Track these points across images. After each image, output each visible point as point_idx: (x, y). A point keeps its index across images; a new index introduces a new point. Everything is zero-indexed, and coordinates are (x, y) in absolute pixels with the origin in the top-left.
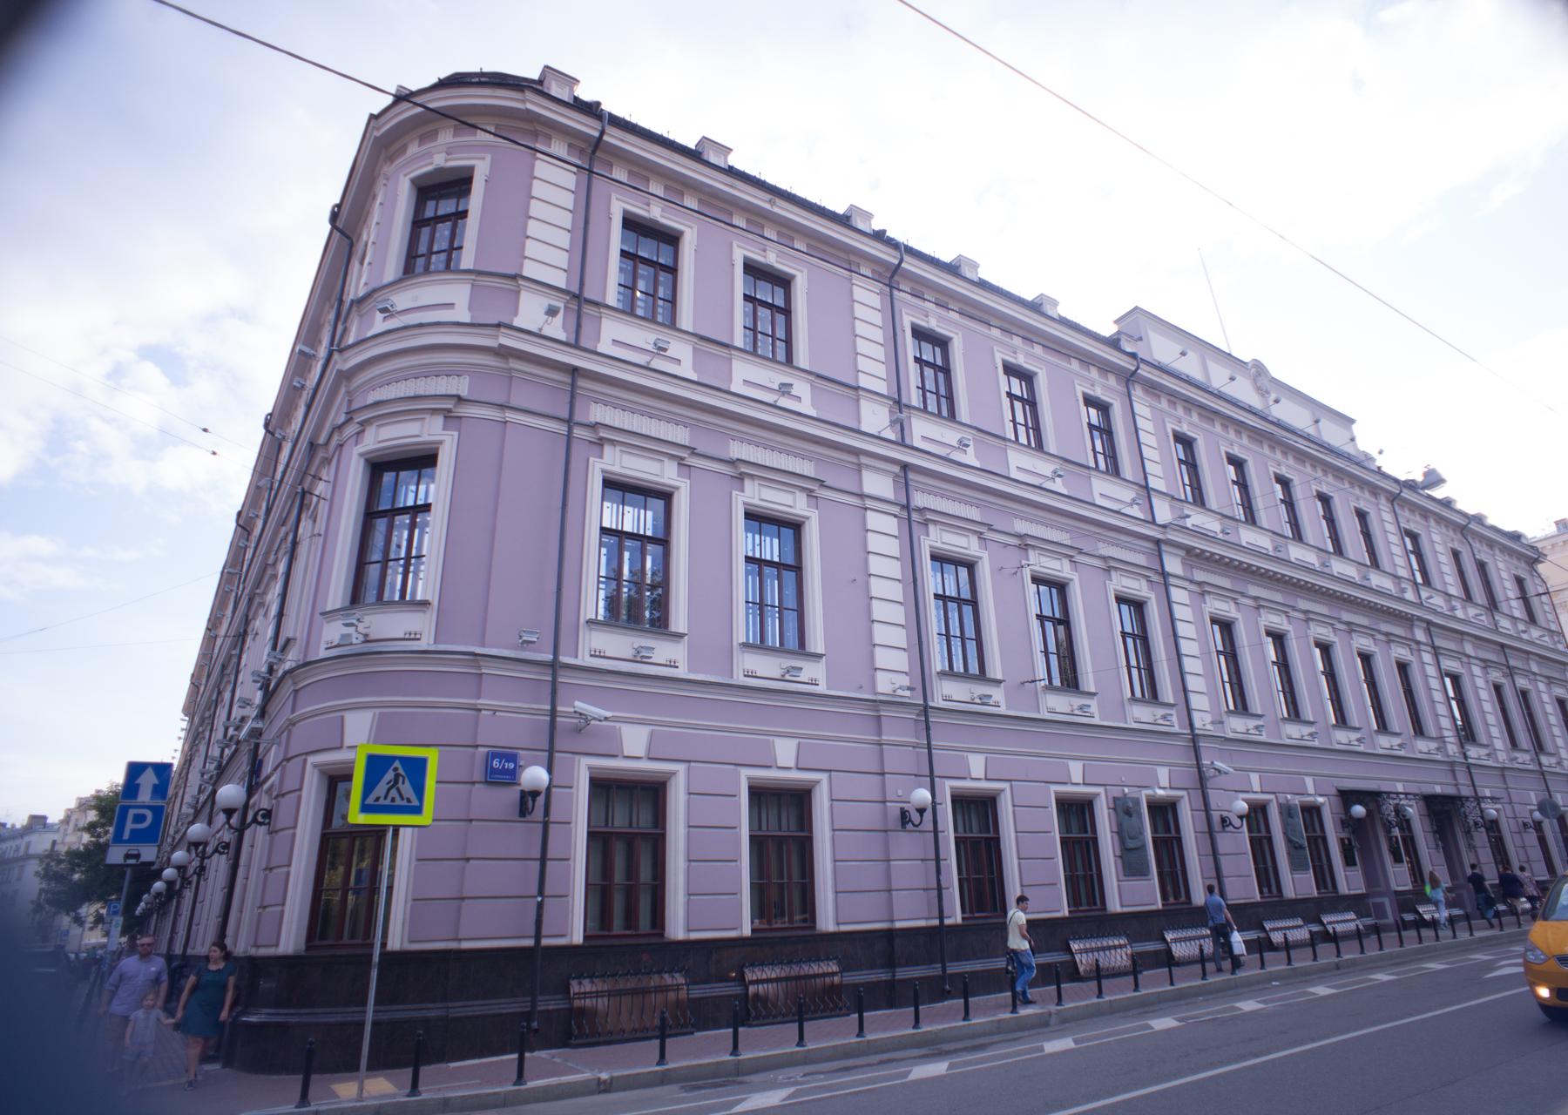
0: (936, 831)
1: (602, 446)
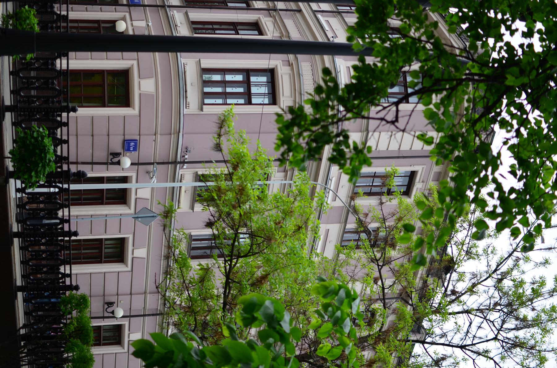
0: (104, 318)
1: (284, 171)
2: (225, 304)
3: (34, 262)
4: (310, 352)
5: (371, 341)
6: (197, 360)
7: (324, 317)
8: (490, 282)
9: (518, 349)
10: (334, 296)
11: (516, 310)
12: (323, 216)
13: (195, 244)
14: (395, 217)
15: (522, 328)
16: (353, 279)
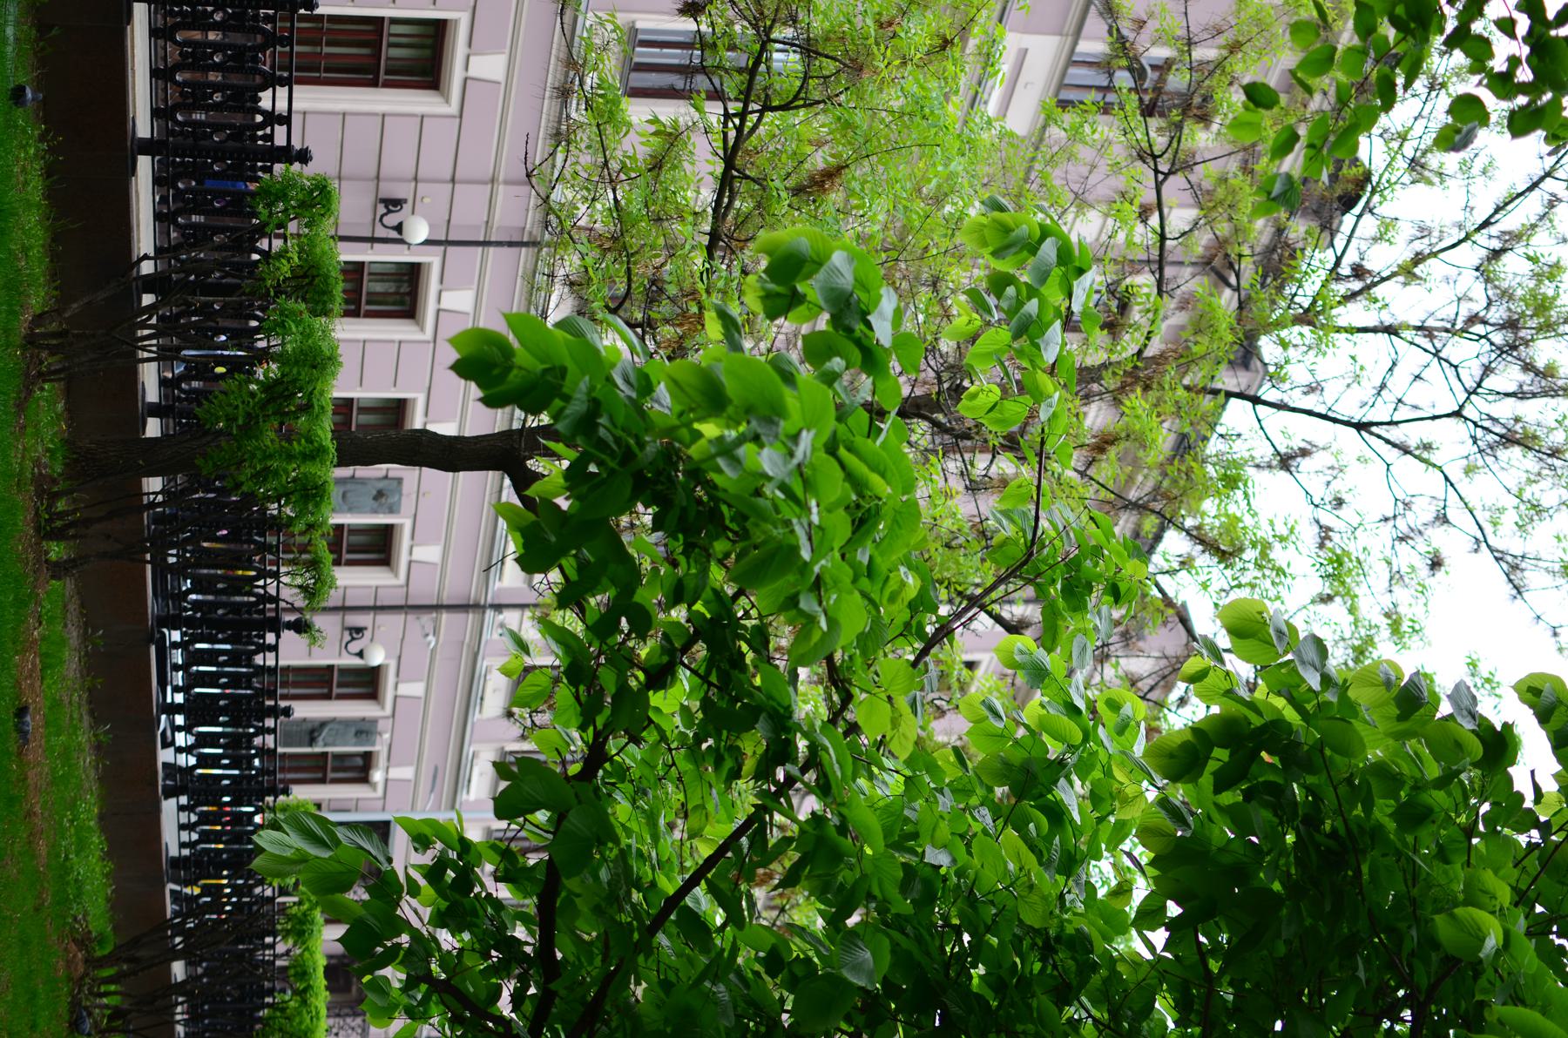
0: (373, 240)
2: (714, 236)
3: (187, 76)
4: (938, 393)
5: (1110, 382)
6: (629, 398)
7: (989, 312)
8: (1470, 255)
9: (1516, 450)
10: (1025, 253)
11: (1527, 343)
12: (1013, 15)
13: (645, 55)
14: (1221, 40)
15: (1534, 395)
16: (1081, 201)
